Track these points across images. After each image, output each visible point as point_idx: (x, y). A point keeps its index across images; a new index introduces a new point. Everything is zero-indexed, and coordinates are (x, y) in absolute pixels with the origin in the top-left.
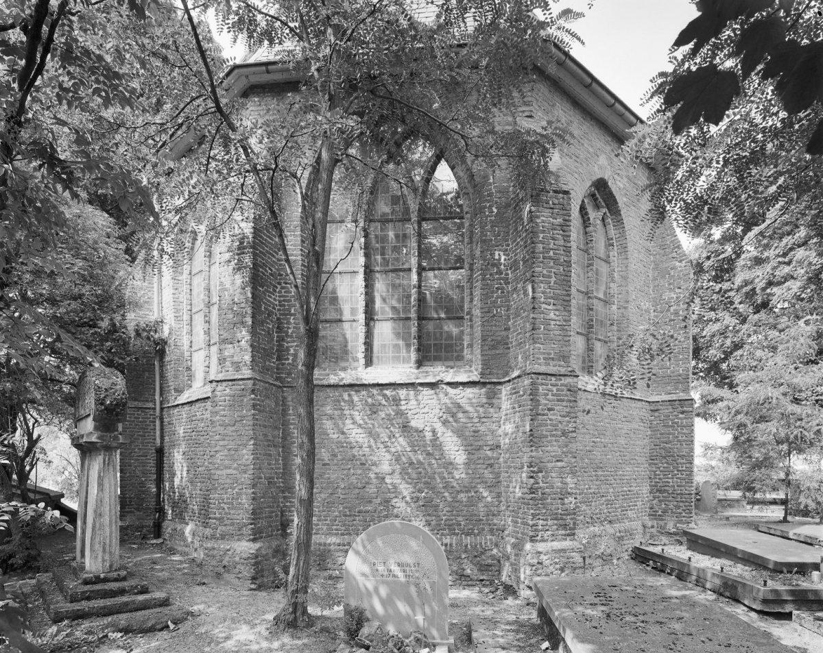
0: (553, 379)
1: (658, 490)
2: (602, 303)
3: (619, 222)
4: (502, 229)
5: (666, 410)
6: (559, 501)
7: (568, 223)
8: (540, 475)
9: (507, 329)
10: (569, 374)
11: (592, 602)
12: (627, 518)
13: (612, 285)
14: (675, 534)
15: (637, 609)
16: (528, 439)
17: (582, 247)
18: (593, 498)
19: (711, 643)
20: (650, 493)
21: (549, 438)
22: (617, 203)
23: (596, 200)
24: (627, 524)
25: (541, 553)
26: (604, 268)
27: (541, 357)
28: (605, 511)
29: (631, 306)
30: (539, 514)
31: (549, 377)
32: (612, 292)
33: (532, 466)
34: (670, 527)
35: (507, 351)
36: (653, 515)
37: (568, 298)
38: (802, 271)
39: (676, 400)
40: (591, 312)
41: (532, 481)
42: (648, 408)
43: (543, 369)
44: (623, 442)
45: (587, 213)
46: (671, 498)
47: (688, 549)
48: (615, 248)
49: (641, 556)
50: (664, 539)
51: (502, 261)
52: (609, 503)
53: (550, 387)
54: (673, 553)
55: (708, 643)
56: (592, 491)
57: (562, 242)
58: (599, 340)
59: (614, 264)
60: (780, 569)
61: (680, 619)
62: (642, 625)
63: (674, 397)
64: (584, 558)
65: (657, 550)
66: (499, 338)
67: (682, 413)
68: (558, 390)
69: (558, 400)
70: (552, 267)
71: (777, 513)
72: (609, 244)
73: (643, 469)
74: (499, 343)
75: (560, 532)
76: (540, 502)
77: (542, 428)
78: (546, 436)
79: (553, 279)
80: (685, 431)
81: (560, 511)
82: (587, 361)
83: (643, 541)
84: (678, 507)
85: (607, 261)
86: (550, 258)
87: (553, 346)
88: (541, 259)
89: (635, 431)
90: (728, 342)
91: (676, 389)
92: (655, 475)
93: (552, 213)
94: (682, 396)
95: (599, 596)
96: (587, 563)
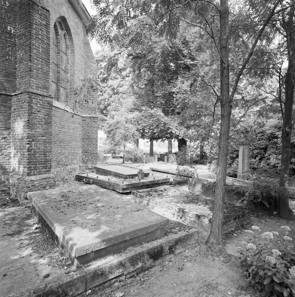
0: (41, 97)
1: (85, 152)
2: (64, 72)
3: (71, 39)
4: (12, 15)
5: (88, 120)
6: (43, 156)
7: (48, 72)
8: (33, 143)
9: (15, 69)
10: (49, 96)
11: (60, 200)
12: (73, 164)
13: (68, 65)
14: (91, 169)
15: (81, 200)
16: (27, 125)
17: (55, 43)
18: (59, 155)
19: (111, 208)
20: (82, 153)
21: (38, 125)
22: (70, 31)
23: (61, 25)
24: (73, 166)
25: (33, 181)
26: (65, 57)
27: (34, 85)
28: (64, 161)
29: (76, 76)
30: (32, 162)
31: (38, 96)
32: (68, 68)
33: (28, 138)
34: (90, 166)
35: (14, 80)
36: (84, 162)
37: (48, 61)
38: (128, 84)
39: (91, 117)
40: (59, 74)
41: (28, 146)
42: (81, 119)
43: (35, 91)
44: (72, 132)
45: (57, 29)
46: (90, 155)
47: (96, 174)
48: (70, 50)
49: (79, 179)
50: (87, 171)
51: (12, 32)
52: (66, 157)
53: (38, 100)
54: (91, 176)
55: (111, 209)
56: (58, 152)
57: (45, 34)
58: (62, 87)
59: (69, 57)
60: (126, 177)
61: (99, 200)
62: (84, 206)
63: (91, 116)
64: (55, 181)
65: (85, 175)
66: (10, 72)
67: (94, 122)
68: (43, 103)
69: (43, 108)
70: (40, 43)
71: (121, 160)
72: (67, 48)
73: (80, 144)
74: (10, 74)
75: (44, 170)
76: (33, 156)
77: (34, 120)
78: (37, 124)
79: (41, 50)
80: (95, 129)
81: (43, 160)
82: (57, 95)
83: (80, 172)
84: (92, 158)
85: (66, 54)
86: (39, 38)
87: (40, 81)
88: (34, 37)
89: (77, 128)
90: (106, 103)
91: (92, 113)
92: (84, 146)
93: (41, 18)
94: (94, 116)
95: (63, 197)
96: (56, 184)
